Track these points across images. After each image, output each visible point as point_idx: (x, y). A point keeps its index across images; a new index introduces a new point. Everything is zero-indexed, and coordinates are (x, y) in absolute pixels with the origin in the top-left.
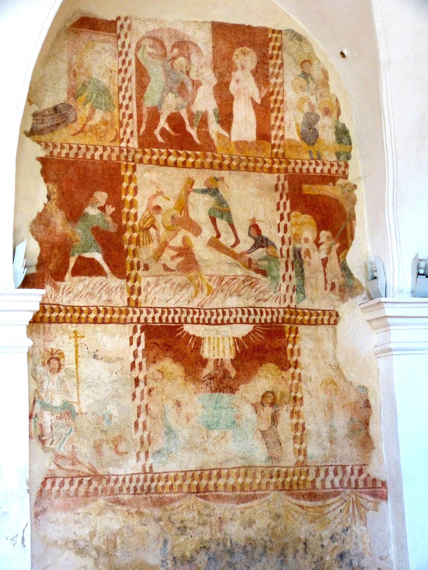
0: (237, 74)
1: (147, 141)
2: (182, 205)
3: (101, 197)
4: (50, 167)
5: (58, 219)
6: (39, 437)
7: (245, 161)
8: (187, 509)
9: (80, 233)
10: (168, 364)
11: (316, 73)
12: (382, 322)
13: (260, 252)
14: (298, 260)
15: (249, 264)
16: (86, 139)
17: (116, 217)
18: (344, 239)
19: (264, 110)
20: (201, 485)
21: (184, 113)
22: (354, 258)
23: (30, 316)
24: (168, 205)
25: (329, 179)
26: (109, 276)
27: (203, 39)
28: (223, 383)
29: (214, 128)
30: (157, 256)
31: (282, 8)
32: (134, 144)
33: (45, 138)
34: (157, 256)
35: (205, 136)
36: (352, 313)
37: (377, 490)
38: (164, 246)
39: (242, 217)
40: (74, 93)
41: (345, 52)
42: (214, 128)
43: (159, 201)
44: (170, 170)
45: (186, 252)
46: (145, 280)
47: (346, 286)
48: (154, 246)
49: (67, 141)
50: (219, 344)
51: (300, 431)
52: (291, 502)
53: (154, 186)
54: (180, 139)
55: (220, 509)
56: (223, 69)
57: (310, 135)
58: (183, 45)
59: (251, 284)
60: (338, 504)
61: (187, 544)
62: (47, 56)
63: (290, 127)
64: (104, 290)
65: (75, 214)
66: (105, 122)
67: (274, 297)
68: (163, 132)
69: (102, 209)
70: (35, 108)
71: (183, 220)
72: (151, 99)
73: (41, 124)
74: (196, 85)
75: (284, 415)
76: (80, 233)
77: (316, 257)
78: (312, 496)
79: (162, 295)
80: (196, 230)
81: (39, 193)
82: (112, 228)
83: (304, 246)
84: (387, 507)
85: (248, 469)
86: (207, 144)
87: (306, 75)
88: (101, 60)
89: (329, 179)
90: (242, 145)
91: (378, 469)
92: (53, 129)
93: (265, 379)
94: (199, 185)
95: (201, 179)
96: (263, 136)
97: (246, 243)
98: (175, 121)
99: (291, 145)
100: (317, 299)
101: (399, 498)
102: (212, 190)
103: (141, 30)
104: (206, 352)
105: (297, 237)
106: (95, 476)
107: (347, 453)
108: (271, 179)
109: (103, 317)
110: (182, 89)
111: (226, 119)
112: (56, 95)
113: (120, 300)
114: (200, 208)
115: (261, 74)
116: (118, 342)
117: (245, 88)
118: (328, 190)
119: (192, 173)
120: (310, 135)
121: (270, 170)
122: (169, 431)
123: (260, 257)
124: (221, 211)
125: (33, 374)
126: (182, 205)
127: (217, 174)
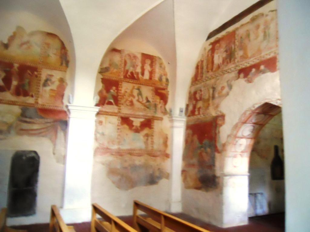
0: (146, 65)
1: (125, 77)
2: (132, 92)
3: (114, 88)
4: (104, 81)
5: (104, 92)
6: (96, 139)
7: (147, 83)
8: (127, 157)
9: (109, 96)
10: (126, 126)
11: (163, 66)
12: (172, 121)
13: (148, 104)
14: (156, 106)
15: (145, 106)
16: (110, 75)
17: (117, 93)
18: (165, 102)
19: (151, 73)
20: (131, 153)
21: (134, 72)
22: (168, 106)
23: (96, 113)
24: (129, 91)
25: (164, 89)
26: (54, 74)
27: (139, 56)
28: (137, 131)
29: (140, 76)
30: (125, 102)
31: (259, 56)
32: (122, 77)
33: (103, 74)
34: (125, 102)
35: (138, 77)
36: (166, 118)
37: (167, 156)
38: (127, 100)
39: (144, 95)
40: (110, 65)
41: (169, 63)
42: (140, 76)
43: (127, 90)
44: (130, 84)
45: (131, 102)
46: (122, 107)
47: (165, 112)
48: (125, 100)
49: (108, 75)
50: (137, 122)
51: (153, 142)
52: (149, 157)
53: (126, 87)
54: (132, 77)
55: (134, 158)
56: (143, 63)
57: (160, 79)
58: (135, 57)
59: (145, 110)
60: (43, 126)
61: (126, 165)
62: (106, 55)
63: (156, 77)
64: (113, 108)
65: (108, 91)
66: (116, 72)
67: (150, 114)
68: (129, 76)
69: (114, 91)
70: (102, 67)
71: (132, 95)
72: (127, 68)
73: (103, 71)
74: (137, 66)
75: (150, 140)
76: (109, 96)
77: (159, 106)
78: (154, 156)
79: (126, 111)
80: (134, 97)
81: (101, 86)
82: (115, 94)
83: (157, 103)
84: (169, 159)
85: (141, 150)
86: (138, 79)
87: (161, 67)
88: (117, 58)
89: (164, 89)
90: (146, 80)
91: (168, 152)
92: (104, 72)
93: (146, 131)
94: (136, 88)
95: (136, 86)
96: (151, 78)
97: (145, 101)
98: (132, 73)
99: (156, 81)
100: (159, 115)
101: (172, 159)
102: (138, 89)
103: (126, 53)
104: (134, 124)
105: (155, 101)
106: (107, 148)
107: (162, 148)
108: (151, 88)
109: (113, 114)
110: (134, 66)
111: (143, 74)
112: (106, 65)
113: (116, 111)
114: (136, 92)
115: (151, 65)
116: (115, 120)
117: (147, 68)
118: (163, 91)
119: (134, 85)
120: (160, 79)
121: (151, 86)
122: (124, 140)
123: (147, 105)
124: (140, 94)
125: (96, 126)
126: (132, 92)
127: (140, 85)
